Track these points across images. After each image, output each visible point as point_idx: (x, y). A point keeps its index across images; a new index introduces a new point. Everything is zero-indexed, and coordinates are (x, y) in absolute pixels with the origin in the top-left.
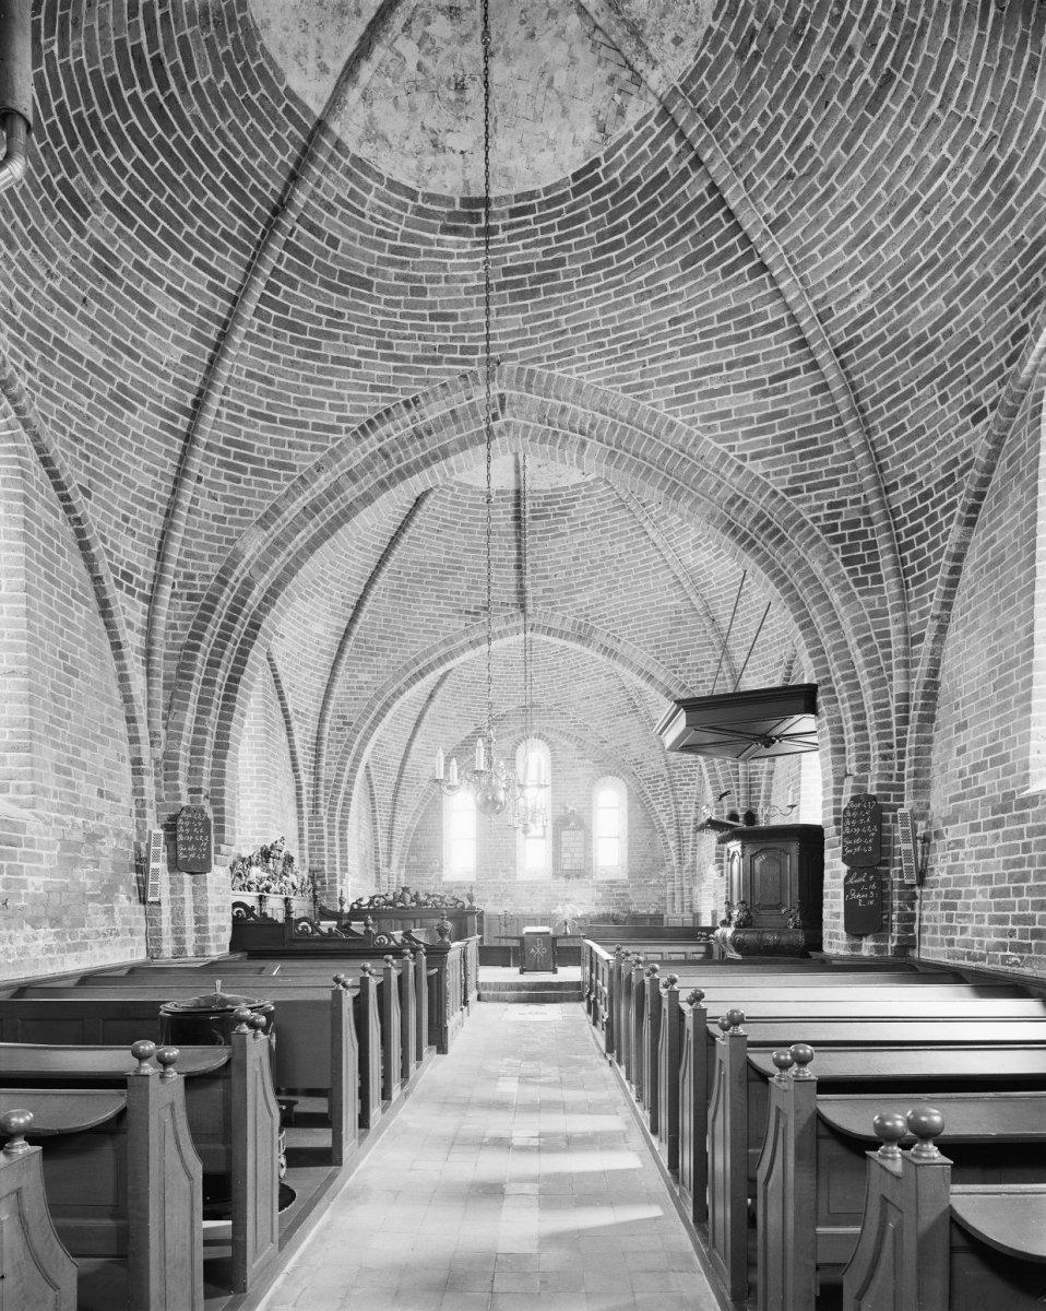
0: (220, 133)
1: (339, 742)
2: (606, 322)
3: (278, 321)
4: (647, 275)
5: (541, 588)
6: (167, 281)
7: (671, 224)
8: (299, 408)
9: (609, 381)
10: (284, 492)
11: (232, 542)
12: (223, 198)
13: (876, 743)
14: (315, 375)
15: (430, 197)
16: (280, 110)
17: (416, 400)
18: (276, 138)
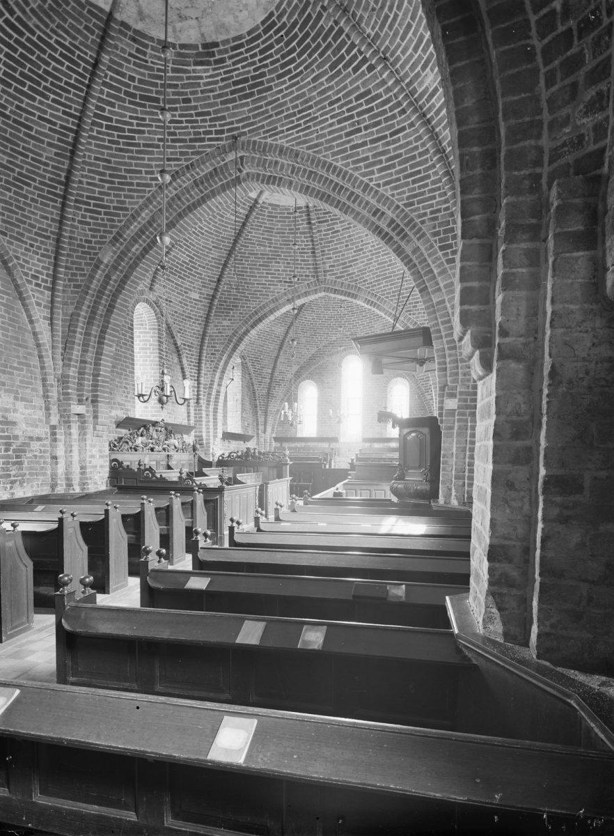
0: (52, 30)
1: (212, 361)
2: (294, 107)
3: (108, 127)
4: (312, 77)
5: (328, 265)
6: (38, 113)
7: (319, 45)
8: (128, 175)
9: (298, 144)
10: (123, 223)
11: (96, 254)
12: (62, 64)
14: (135, 155)
15: (183, 46)
16: (85, 12)
17: (192, 165)
18: (86, 28)
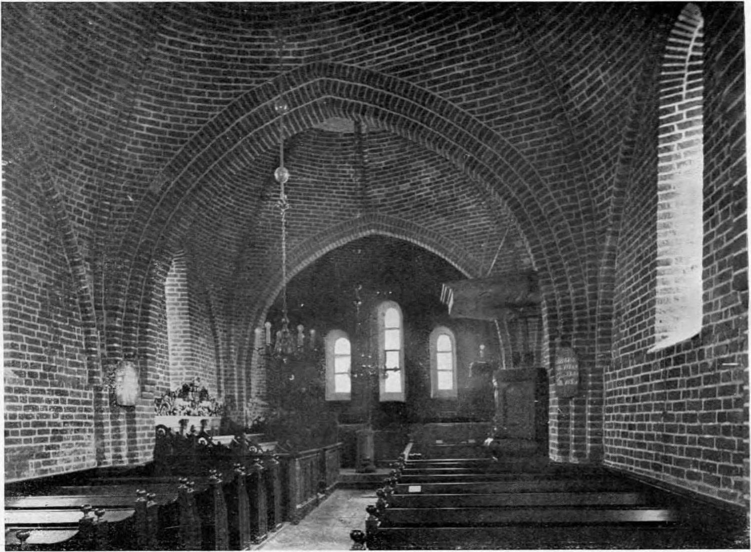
10: (180, 151)
13: (574, 451)
